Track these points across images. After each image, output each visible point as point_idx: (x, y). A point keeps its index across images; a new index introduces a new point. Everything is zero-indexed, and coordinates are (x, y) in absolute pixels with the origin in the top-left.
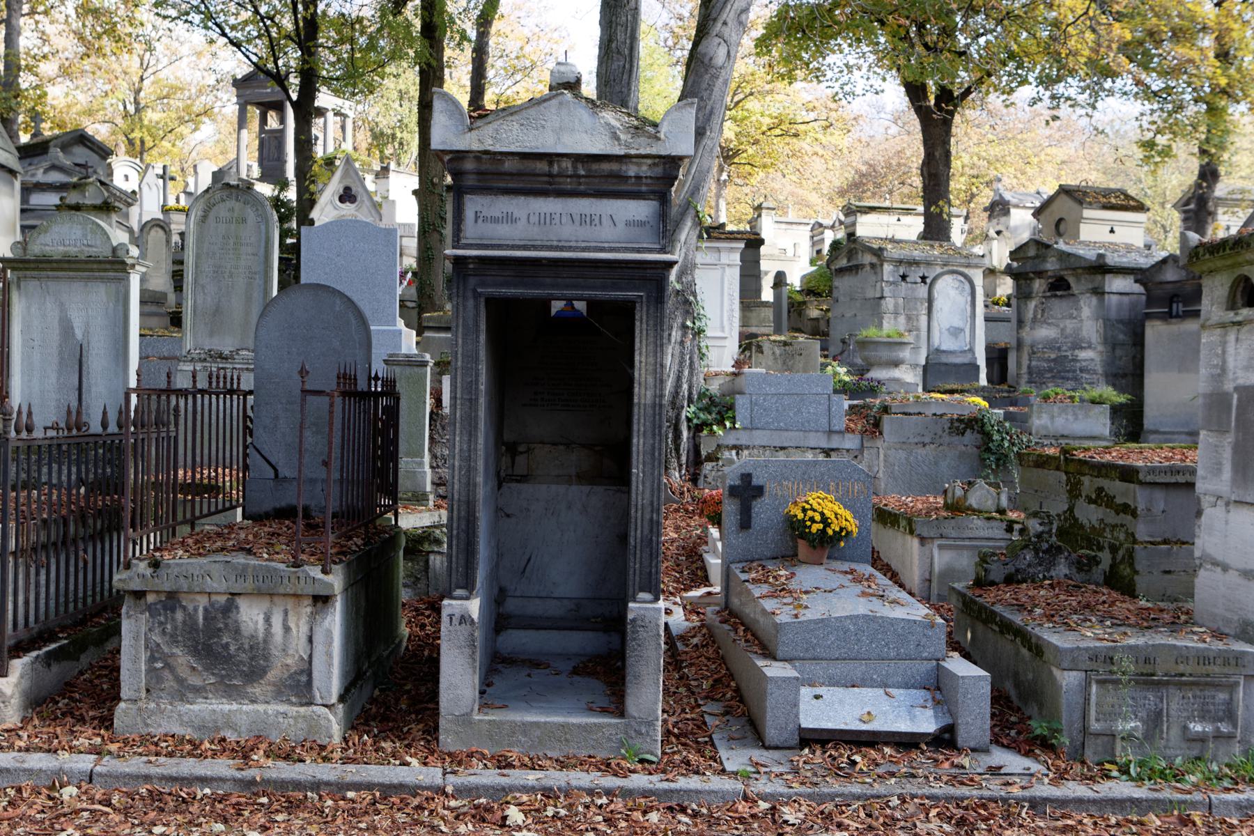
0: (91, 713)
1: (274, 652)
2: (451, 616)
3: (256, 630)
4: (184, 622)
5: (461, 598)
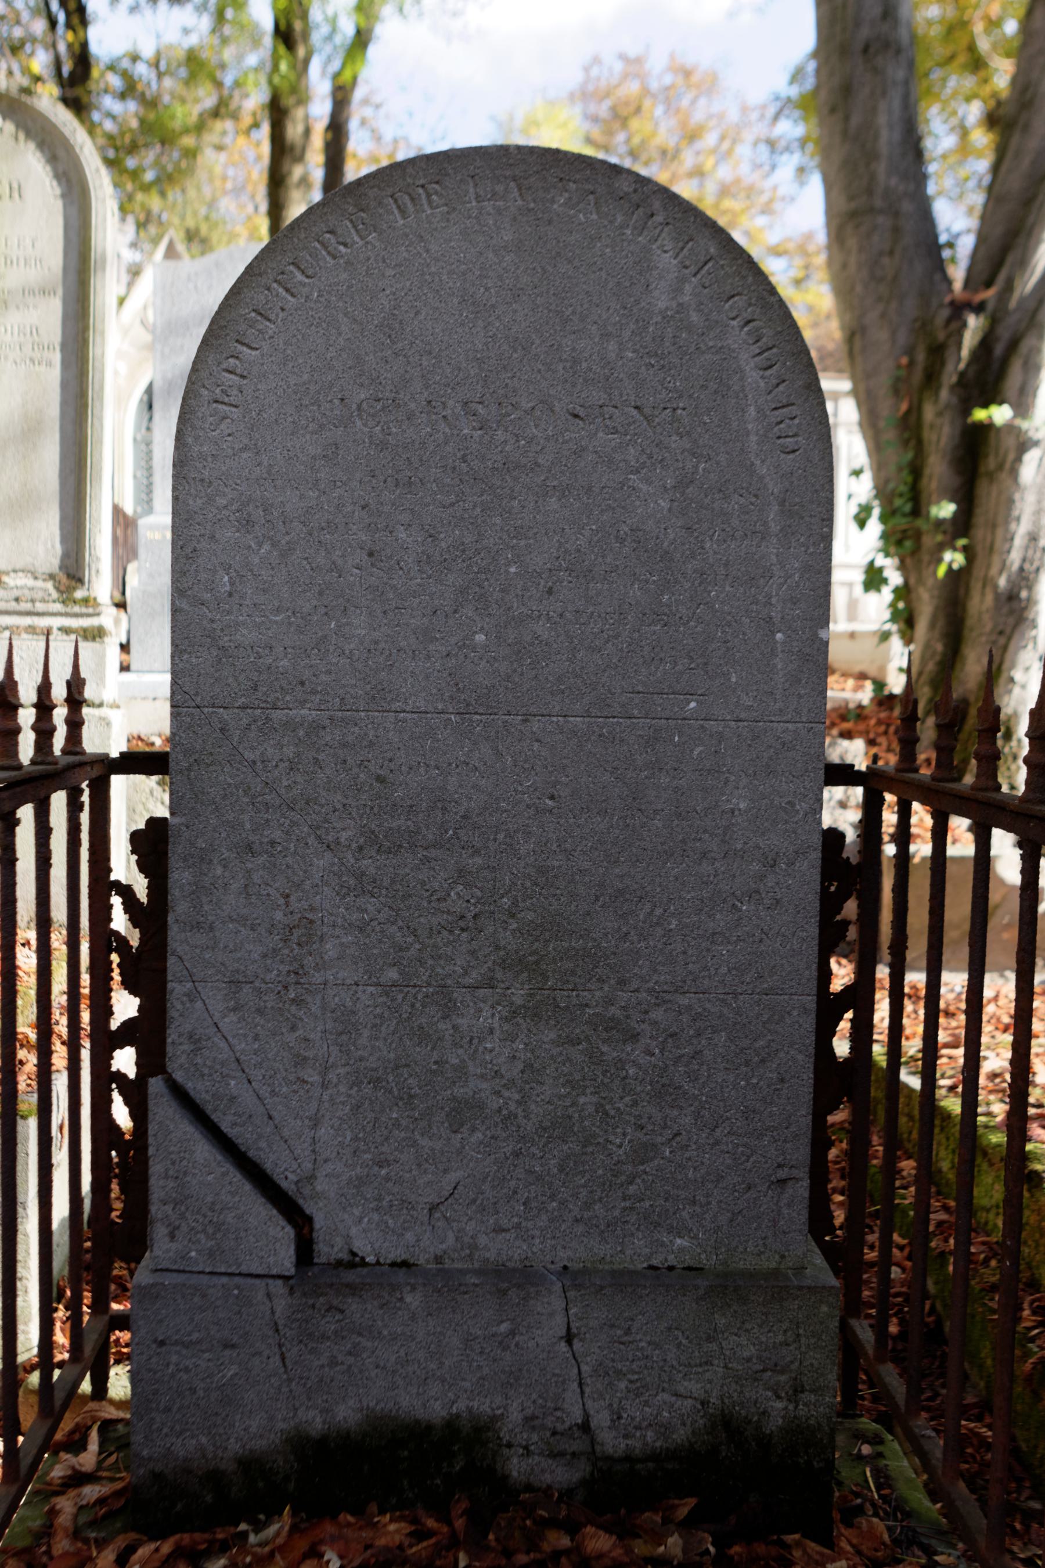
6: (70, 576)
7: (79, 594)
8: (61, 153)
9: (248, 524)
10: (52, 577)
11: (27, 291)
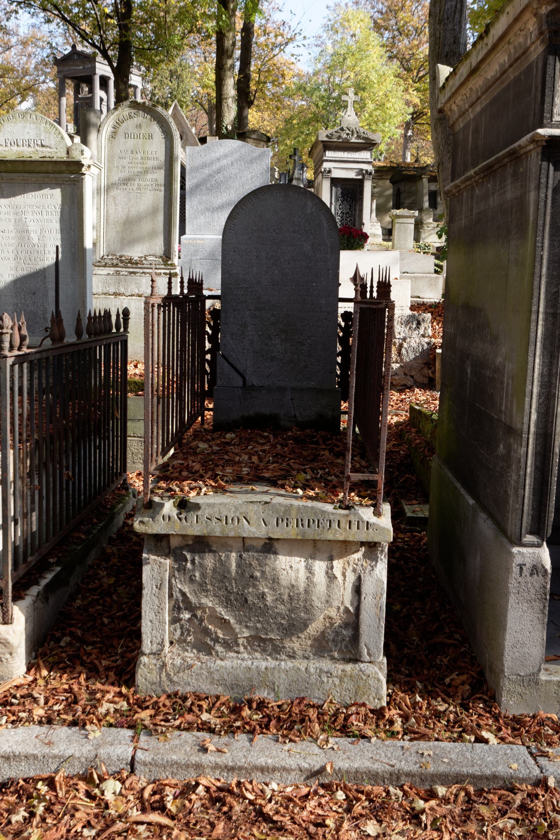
0: (104, 663)
1: (317, 603)
2: (521, 567)
3: (297, 578)
4: (214, 570)
5: (532, 545)
6: (167, 257)
7: (169, 263)
8: (164, 125)
9: (235, 251)
10: (161, 257)
11: (154, 168)
